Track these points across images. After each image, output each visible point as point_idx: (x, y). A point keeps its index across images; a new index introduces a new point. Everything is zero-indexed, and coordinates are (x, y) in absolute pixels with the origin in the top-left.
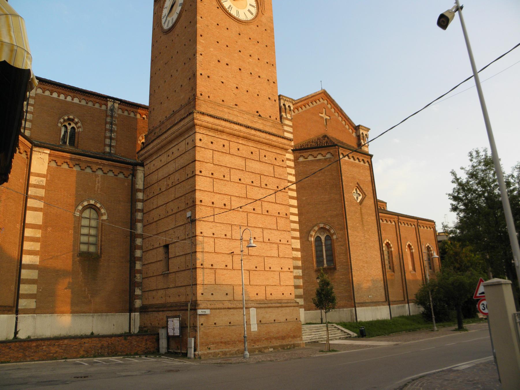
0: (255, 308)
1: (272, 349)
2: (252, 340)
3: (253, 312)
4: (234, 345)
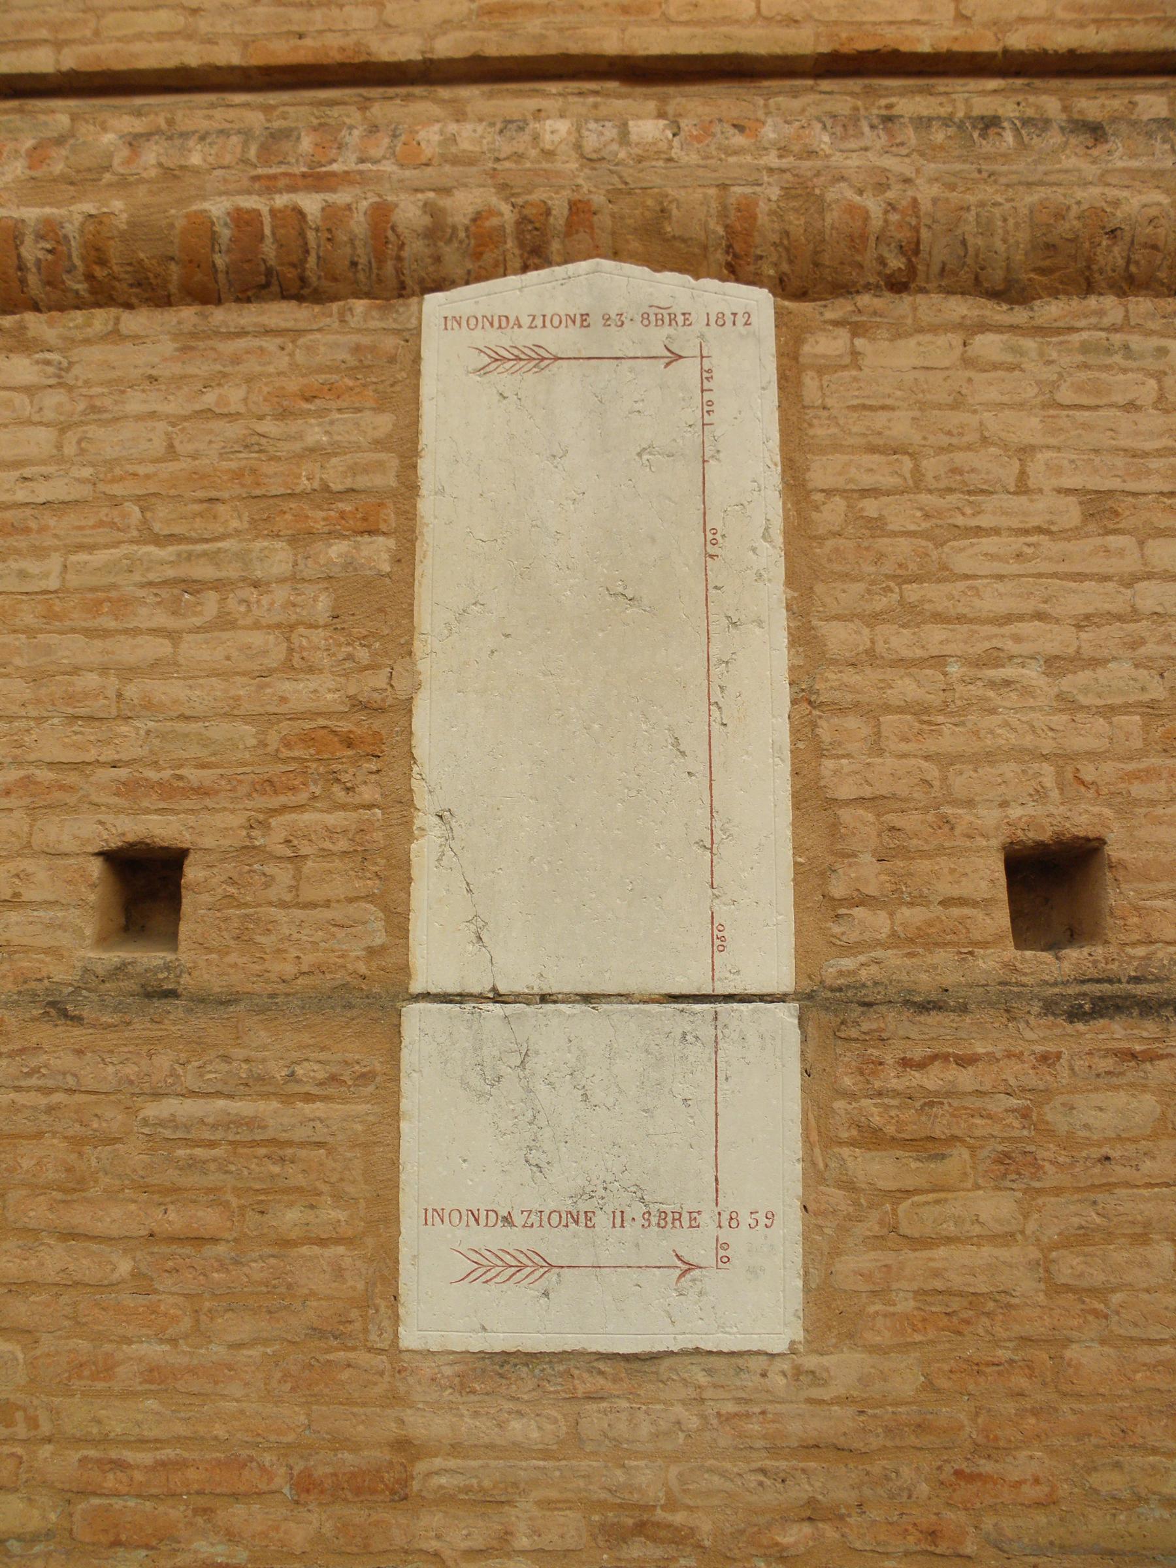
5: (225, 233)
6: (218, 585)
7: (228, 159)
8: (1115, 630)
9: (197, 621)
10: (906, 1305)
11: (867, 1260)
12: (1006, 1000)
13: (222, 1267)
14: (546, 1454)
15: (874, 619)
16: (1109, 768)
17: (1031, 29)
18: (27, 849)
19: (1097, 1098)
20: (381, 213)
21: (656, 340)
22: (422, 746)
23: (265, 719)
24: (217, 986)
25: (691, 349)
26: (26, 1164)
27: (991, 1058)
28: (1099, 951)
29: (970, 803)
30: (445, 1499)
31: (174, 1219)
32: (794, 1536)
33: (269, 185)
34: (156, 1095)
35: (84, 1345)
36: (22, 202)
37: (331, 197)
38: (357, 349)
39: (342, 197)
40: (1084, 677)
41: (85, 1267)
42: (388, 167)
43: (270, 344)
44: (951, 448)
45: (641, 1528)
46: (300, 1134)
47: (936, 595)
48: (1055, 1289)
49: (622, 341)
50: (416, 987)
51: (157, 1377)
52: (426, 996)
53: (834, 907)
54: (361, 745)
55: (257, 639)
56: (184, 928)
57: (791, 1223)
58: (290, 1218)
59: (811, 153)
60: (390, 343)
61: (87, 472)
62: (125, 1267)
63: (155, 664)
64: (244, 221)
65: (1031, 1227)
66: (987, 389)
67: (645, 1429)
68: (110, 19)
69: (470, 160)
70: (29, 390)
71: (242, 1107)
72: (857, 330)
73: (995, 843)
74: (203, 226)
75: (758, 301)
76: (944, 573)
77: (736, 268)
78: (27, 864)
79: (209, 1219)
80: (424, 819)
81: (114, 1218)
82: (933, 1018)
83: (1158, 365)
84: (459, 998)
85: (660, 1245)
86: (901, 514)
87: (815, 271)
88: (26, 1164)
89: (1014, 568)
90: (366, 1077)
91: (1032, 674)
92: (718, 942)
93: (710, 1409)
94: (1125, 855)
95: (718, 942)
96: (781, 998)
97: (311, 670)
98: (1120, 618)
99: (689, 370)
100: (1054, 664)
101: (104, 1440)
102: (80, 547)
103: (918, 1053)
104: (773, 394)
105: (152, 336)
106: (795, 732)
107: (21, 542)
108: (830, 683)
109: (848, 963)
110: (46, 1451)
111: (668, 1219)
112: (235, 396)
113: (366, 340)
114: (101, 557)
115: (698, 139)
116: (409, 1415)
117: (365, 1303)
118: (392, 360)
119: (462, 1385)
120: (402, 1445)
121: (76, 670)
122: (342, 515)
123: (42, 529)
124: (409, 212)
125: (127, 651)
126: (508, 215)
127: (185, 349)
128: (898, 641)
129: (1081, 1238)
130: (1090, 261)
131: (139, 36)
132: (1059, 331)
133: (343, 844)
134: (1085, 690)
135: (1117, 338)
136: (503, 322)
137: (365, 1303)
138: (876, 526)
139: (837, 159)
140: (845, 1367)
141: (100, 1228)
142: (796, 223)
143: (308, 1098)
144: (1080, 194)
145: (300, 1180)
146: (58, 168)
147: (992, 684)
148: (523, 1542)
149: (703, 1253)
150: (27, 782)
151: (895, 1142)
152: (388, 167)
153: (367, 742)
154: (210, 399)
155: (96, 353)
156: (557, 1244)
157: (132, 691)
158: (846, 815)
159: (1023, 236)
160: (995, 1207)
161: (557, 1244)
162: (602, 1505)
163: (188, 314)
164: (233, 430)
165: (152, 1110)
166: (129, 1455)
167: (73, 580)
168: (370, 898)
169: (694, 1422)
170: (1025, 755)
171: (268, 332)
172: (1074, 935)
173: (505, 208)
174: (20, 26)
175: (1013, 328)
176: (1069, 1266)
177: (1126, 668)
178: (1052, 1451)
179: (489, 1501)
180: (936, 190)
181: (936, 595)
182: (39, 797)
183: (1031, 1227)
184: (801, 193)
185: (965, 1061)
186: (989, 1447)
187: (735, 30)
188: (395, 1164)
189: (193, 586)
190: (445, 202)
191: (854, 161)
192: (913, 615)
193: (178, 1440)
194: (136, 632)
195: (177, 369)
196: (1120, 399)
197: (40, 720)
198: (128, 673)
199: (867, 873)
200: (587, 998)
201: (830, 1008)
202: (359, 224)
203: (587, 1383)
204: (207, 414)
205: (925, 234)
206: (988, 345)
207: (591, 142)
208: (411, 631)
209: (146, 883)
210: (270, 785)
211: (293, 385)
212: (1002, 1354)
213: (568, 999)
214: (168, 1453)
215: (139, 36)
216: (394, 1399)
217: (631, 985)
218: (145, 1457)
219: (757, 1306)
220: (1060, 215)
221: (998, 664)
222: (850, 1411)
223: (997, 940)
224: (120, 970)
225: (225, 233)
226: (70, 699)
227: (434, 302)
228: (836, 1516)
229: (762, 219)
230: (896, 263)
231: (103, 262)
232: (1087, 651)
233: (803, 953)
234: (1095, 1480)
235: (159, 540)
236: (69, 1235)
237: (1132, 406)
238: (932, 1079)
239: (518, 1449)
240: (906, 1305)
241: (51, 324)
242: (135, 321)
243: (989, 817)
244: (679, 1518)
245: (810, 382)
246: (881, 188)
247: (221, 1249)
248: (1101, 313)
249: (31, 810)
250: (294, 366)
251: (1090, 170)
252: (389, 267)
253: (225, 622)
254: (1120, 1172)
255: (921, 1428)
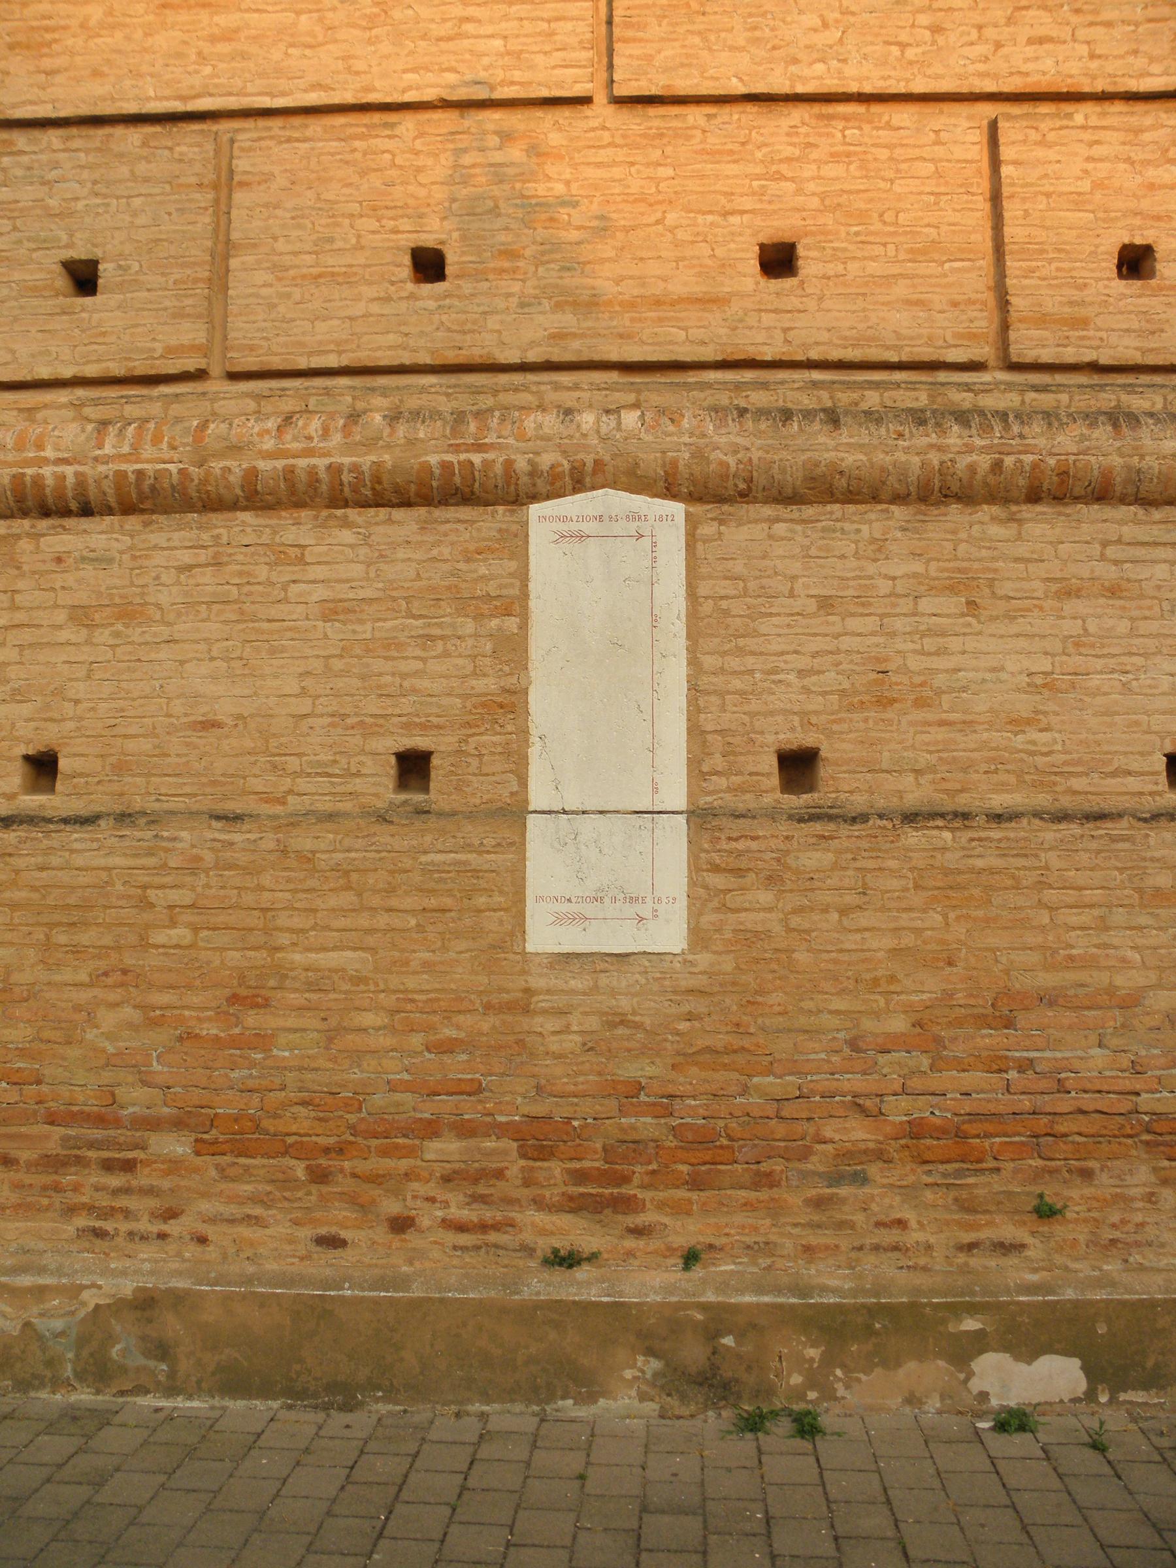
0: (668, 487)
1: (1056, 1377)
2: (538, 1140)
3: (607, 602)
4: (93, 1183)
5: (437, 472)
6: (442, 638)
7: (437, 435)
8: (830, 658)
9: (434, 653)
10: (728, 935)
11: (714, 917)
12: (772, 815)
13: (454, 921)
14: (585, 994)
15: (724, 654)
16: (824, 718)
17: (821, 348)
18: (363, 751)
19: (809, 854)
20: (509, 463)
21: (632, 527)
22: (532, 708)
23: (465, 697)
24: (447, 808)
25: (647, 533)
26: (371, 881)
27: (765, 837)
28: (816, 795)
29: (762, 733)
30: (544, 1012)
31: (433, 902)
32: (683, 1026)
33: (456, 449)
34: (425, 852)
35: (397, 954)
36: (342, 455)
37: (485, 456)
38: (500, 531)
39: (490, 456)
40: (814, 678)
41: (397, 921)
42: (511, 441)
43: (461, 527)
44: (761, 577)
45: (622, 1022)
46: (486, 867)
47: (751, 643)
48: (789, 930)
49: (617, 528)
50: (531, 808)
51: (427, 966)
52: (535, 812)
53: (704, 776)
54: (505, 709)
55: (460, 662)
56: (432, 785)
57: (683, 902)
58: (481, 901)
59: (704, 436)
60: (514, 528)
61: (380, 585)
62: (413, 922)
63: (417, 672)
64: (446, 466)
65: (780, 905)
66: (779, 549)
67: (624, 983)
68: (365, 338)
69: (547, 439)
70: (351, 546)
71: (459, 856)
72: (722, 522)
73: (772, 749)
74: (427, 468)
75: (677, 508)
76: (756, 634)
77: (670, 491)
78: (362, 758)
79: (448, 902)
80: (534, 739)
81: (409, 902)
82: (742, 821)
83: (857, 537)
84: (550, 812)
85: (630, 910)
86: (737, 607)
87: (708, 492)
88: (371, 881)
89: (786, 631)
90: (512, 844)
91: (792, 677)
92: (655, 790)
93: (650, 976)
94: (829, 755)
95: (655, 790)
96: (681, 813)
97: (484, 675)
98: (831, 653)
99: (646, 542)
100: (801, 673)
101: (406, 991)
102: (379, 620)
103: (735, 835)
104: (683, 553)
105: (406, 522)
106: (689, 703)
107: (352, 617)
108: (705, 681)
109: (709, 799)
110: (382, 995)
111: (633, 900)
112: (446, 551)
113: (504, 526)
114: (389, 624)
115: (653, 427)
116: (529, 979)
117: (512, 934)
118: (516, 536)
119: (551, 966)
120: (527, 991)
121: (381, 675)
122: (496, 607)
123: (362, 611)
124: (521, 464)
125: (403, 666)
126: (566, 465)
127: (423, 528)
128: (734, 663)
129: (799, 910)
130: (831, 485)
131: (379, 348)
132: (812, 522)
133: (500, 749)
134: (814, 684)
135: (838, 525)
136: (565, 519)
137: (512, 934)
138: (726, 613)
139: (716, 438)
140: (704, 959)
141: (402, 907)
142: (697, 470)
143: (488, 852)
144: (826, 455)
145: (485, 886)
146: (358, 438)
147: (773, 682)
148: (575, 1028)
149: (647, 914)
150: (362, 722)
151: (725, 870)
152: (511, 441)
153: (510, 705)
154: (435, 552)
155: (381, 529)
156: (589, 910)
157: (406, 684)
158: (709, 737)
159: (800, 475)
160: (765, 897)
161: (589, 910)
162: (607, 1014)
163: (423, 510)
164: (446, 567)
165: (423, 859)
166: (416, 997)
167: (378, 635)
168: (511, 771)
169: (643, 981)
170: (786, 712)
171: (459, 521)
172: (811, 788)
173: (565, 462)
174: (320, 343)
175: (792, 521)
176: (795, 921)
177: (833, 674)
178: (786, 993)
179: (561, 1013)
180: (760, 453)
181: (751, 643)
182: (368, 729)
183: (780, 905)
184: (699, 454)
185: (754, 838)
186: (760, 992)
187: (676, 348)
188: (524, 878)
189: (431, 638)
190: (537, 459)
191: (723, 440)
192: (741, 652)
193: (437, 990)
194: (406, 658)
195: (419, 538)
196: (837, 553)
197: (366, 696)
198: (404, 676)
199: (718, 762)
200: (601, 812)
201: (700, 817)
202: (498, 468)
203: (601, 965)
204: (434, 559)
205: (755, 474)
206: (780, 528)
207: (604, 429)
208: (527, 658)
209: (413, 767)
210: (468, 724)
211: (472, 547)
212: (767, 955)
213: (593, 812)
214: (433, 995)
215: (379, 348)
216: (524, 972)
217: (620, 808)
218: (423, 997)
219: (669, 935)
220: (817, 464)
221: (777, 673)
222: (705, 977)
223: (772, 790)
224: (405, 802)
225: (437, 472)
226: (379, 687)
227: (535, 509)
228: (699, 1018)
229: (681, 468)
230: (742, 486)
231: (380, 483)
232: (816, 667)
233: (690, 795)
234: (802, 1004)
235: (414, 617)
236: (390, 910)
237: (843, 557)
238: (741, 845)
239: (573, 992)
240: (728, 935)
241: (359, 514)
242: (399, 514)
243: (770, 738)
244: (637, 1019)
245: (700, 546)
246: (736, 452)
247: (453, 914)
248: (831, 513)
249: (364, 735)
250: (472, 537)
251: (831, 443)
252: (512, 488)
253: (446, 654)
254: (817, 884)
255: (734, 984)
